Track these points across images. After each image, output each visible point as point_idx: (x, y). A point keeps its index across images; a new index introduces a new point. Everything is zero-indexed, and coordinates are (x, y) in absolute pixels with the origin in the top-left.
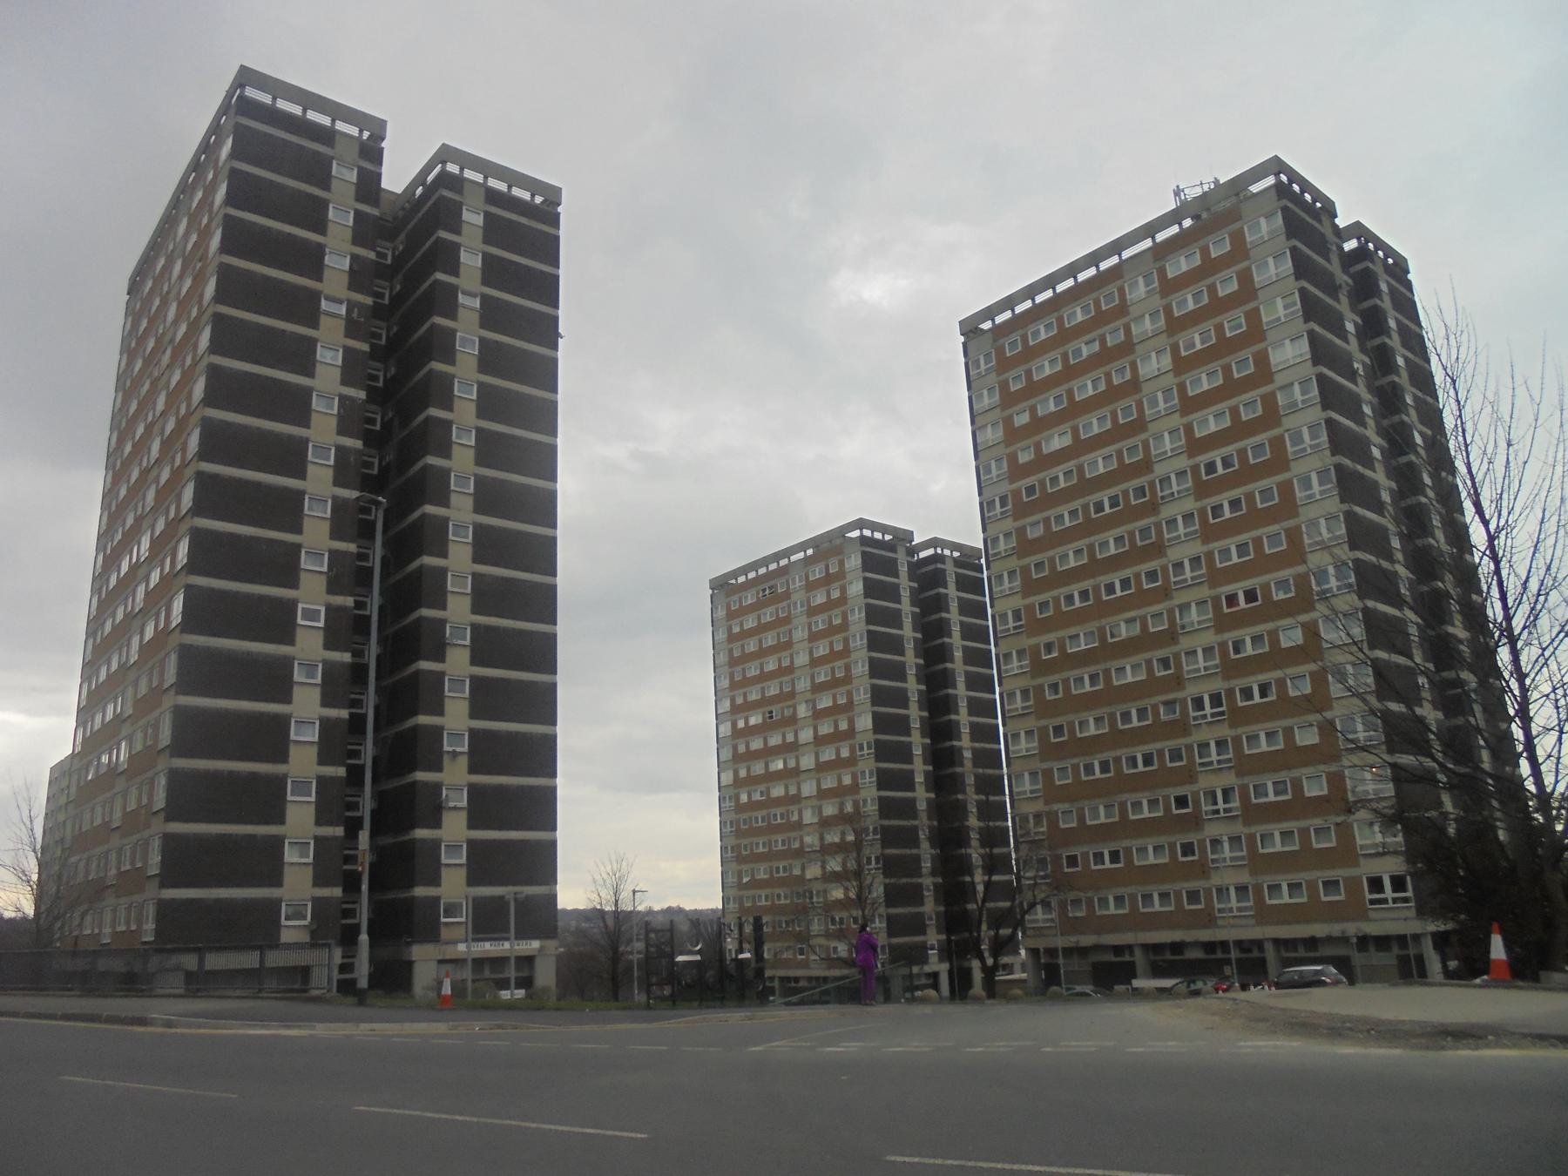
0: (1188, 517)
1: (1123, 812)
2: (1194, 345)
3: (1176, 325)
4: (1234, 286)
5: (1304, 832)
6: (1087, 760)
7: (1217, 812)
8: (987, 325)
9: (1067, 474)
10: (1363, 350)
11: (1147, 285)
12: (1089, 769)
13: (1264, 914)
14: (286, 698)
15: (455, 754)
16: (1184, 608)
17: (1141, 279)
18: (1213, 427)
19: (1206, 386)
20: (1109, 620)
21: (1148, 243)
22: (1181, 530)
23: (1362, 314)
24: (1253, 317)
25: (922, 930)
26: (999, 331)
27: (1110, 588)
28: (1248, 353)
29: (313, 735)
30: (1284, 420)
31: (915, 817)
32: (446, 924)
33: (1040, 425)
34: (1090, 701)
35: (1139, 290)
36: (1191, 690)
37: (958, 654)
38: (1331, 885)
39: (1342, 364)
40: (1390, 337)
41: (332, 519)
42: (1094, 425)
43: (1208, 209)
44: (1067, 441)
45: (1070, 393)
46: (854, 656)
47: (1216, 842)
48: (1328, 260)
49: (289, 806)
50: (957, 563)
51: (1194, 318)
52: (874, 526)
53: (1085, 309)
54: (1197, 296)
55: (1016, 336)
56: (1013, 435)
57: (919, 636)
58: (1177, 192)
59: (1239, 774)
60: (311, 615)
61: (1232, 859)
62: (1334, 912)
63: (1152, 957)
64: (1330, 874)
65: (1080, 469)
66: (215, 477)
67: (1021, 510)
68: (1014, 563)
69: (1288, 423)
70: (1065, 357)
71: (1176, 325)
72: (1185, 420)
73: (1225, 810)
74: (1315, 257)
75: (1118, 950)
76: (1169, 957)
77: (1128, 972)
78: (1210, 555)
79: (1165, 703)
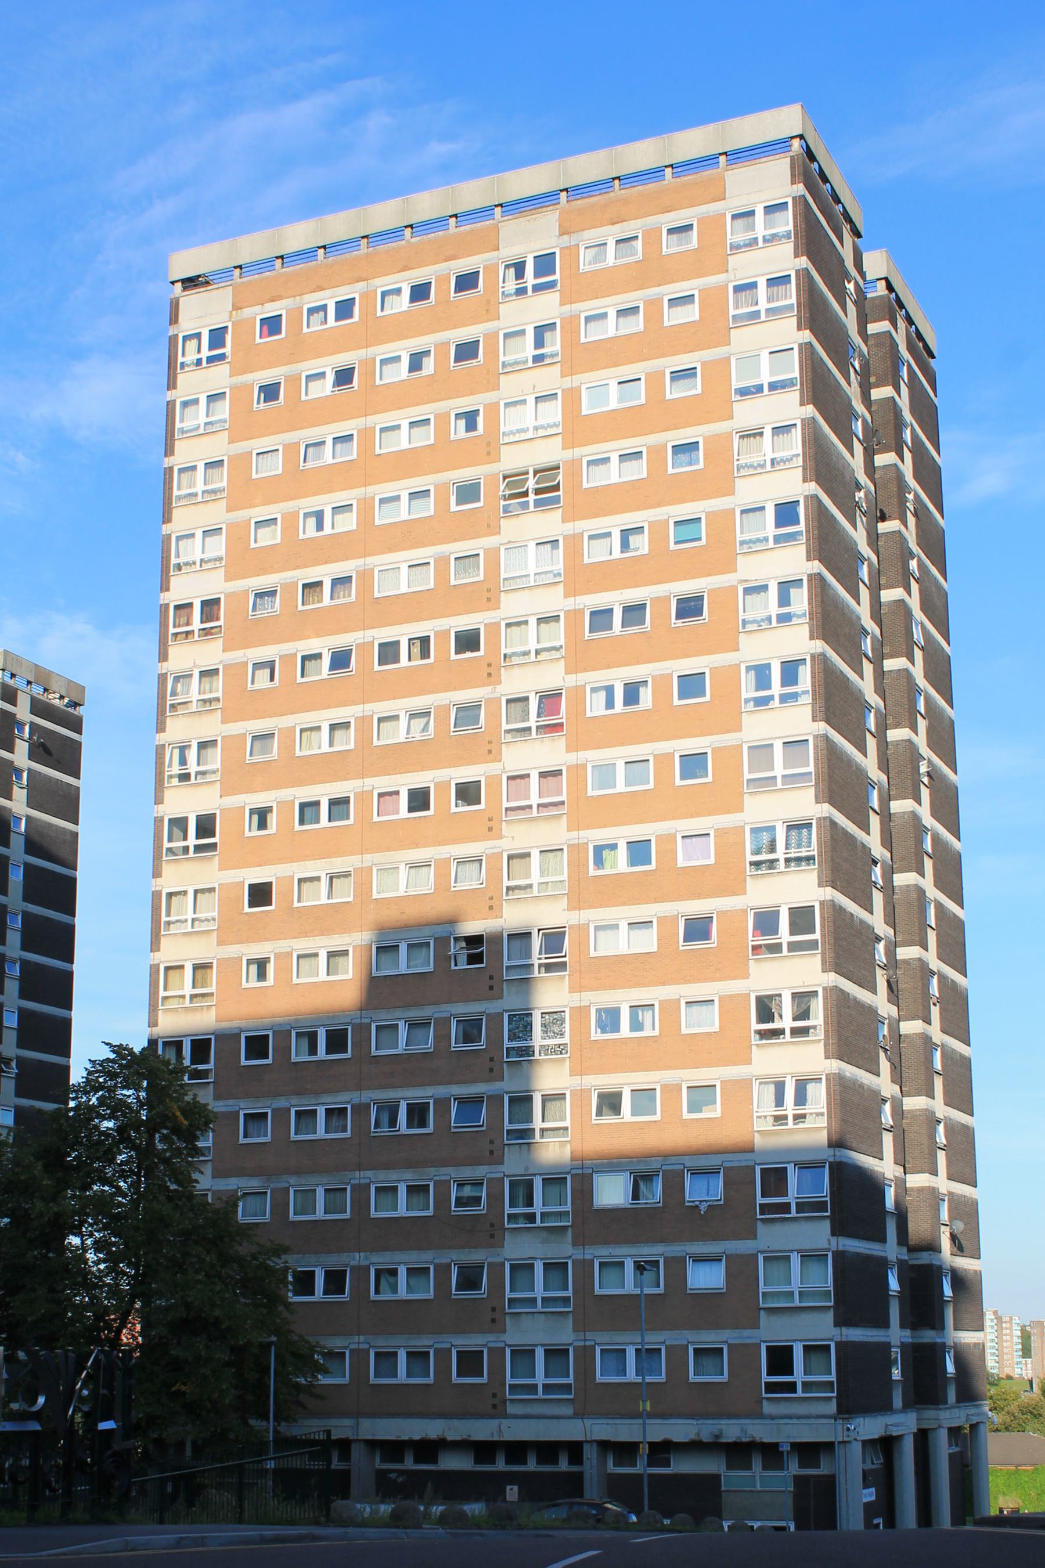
7: (531, 1218)
13: (591, 1400)
32: (512, 1401)
38: (707, 1354)
62: (709, 1402)
63: (379, 1465)
64: (709, 1338)
76: (409, 1463)
77: (340, 1485)
79: (462, 1101)
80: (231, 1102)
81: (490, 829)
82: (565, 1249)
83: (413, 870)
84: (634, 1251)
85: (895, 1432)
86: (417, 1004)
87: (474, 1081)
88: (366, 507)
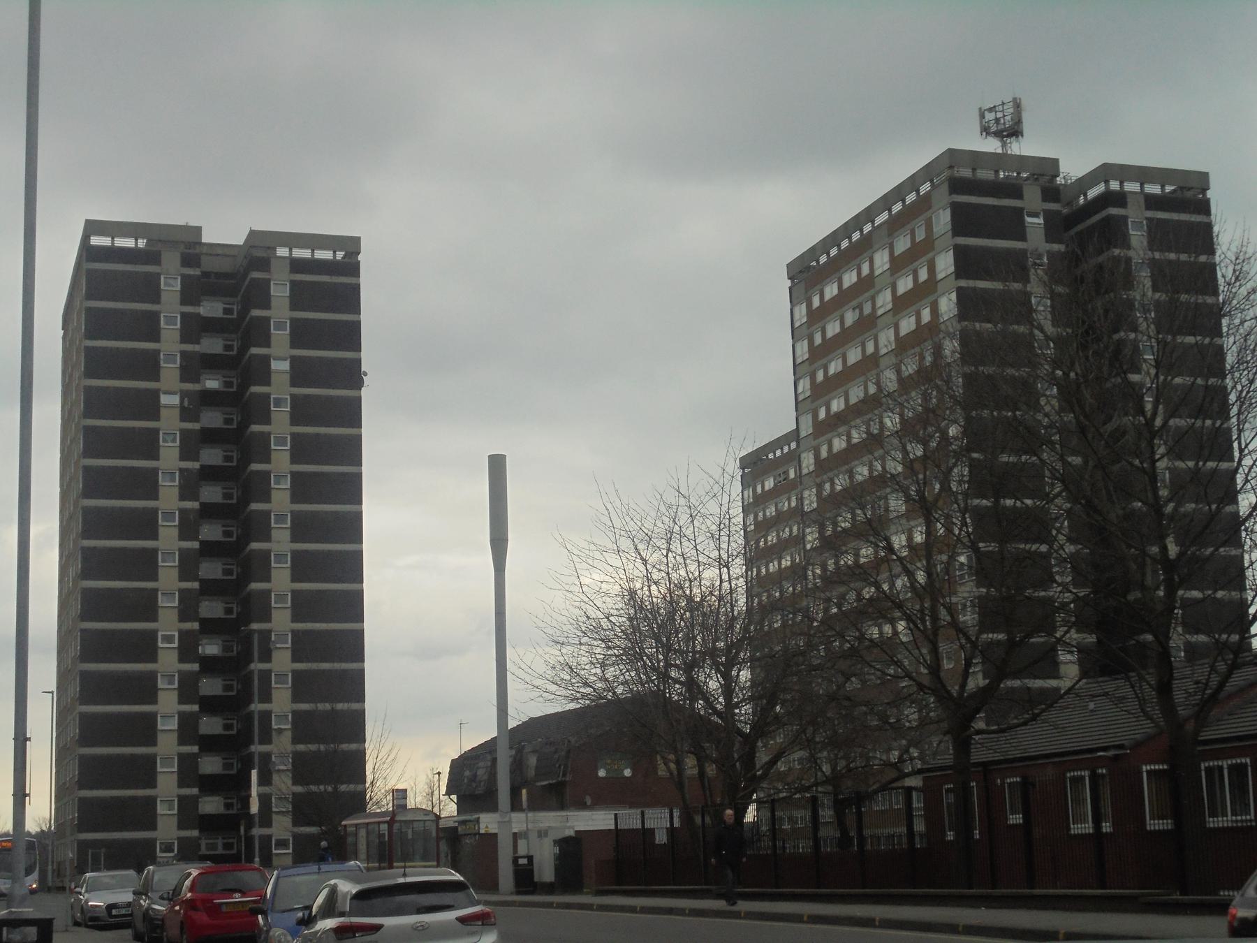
14: (154, 701)
15: (280, 731)
29: (173, 725)
32: (277, 855)
41: (180, 566)
49: (160, 652)
60: (169, 639)
66: (94, 428)
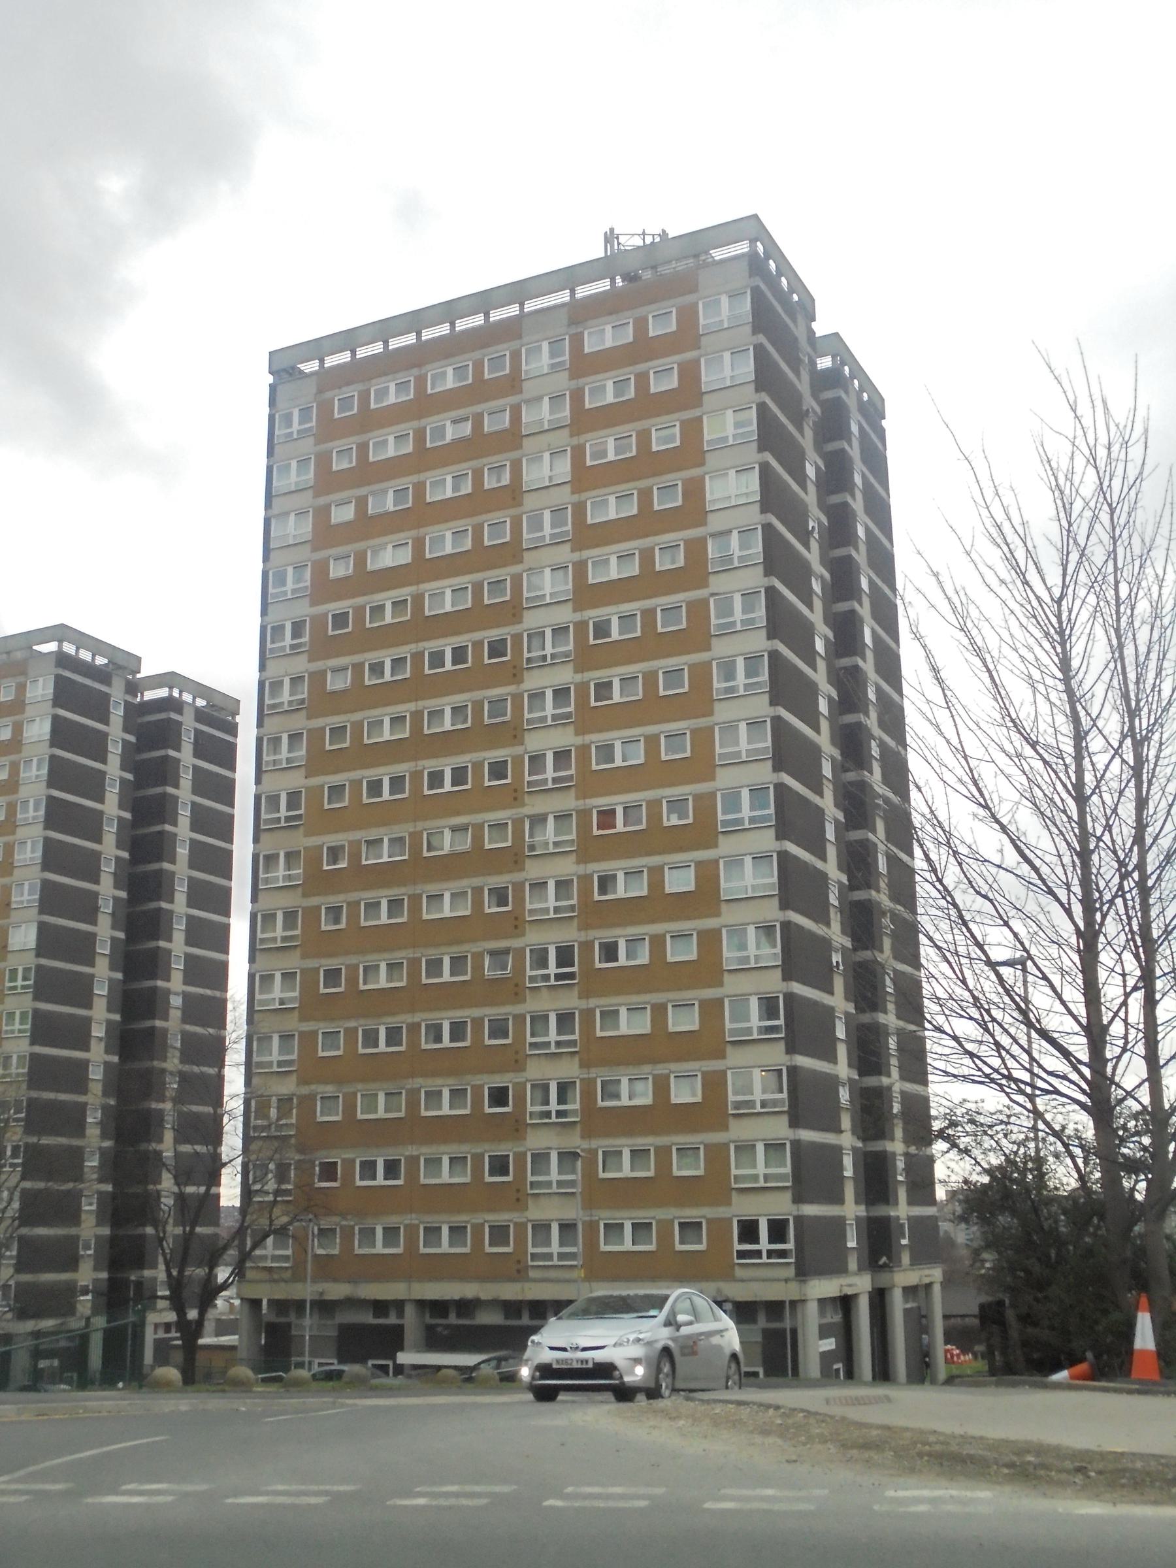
0: (561, 694)
1: (413, 1104)
2: (604, 453)
3: (585, 420)
4: (672, 382)
5: (663, 1153)
6: (370, 1024)
7: (548, 1114)
8: (311, 367)
9: (398, 605)
10: (821, 505)
11: (553, 355)
12: (371, 1038)
16: (539, 820)
17: (545, 346)
18: (614, 572)
19: (612, 515)
20: (429, 824)
21: (563, 297)
22: (550, 709)
23: (825, 456)
24: (692, 430)
25: (72, 1263)
26: (330, 379)
27: (436, 779)
28: (677, 479)
30: (712, 579)
31: (85, 1091)
32: (533, 1266)
33: (369, 526)
34: (384, 938)
35: (540, 361)
36: (533, 938)
37: (183, 852)
38: (690, 1228)
39: (795, 517)
40: (853, 496)
42: (447, 541)
43: (654, 267)
44: (405, 557)
45: (420, 488)
46: (21, 833)
47: (540, 1159)
48: (798, 374)
50: (201, 716)
51: (609, 417)
52: (82, 640)
53: (460, 371)
54: (619, 385)
55: (353, 391)
56: (326, 534)
57: (127, 815)
58: (610, 237)
59: (585, 1065)
61: (560, 1184)
63: (429, 1320)
64: (691, 1214)
65: (418, 599)
67: (324, 646)
68: (300, 722)
69: (718, 584)
70: (420, 436)
71: (585, 420)
72: (576, 556)
73: (560, 1114)
74: (783, 365)
75: (380, 1307)
77: (393, 1340)
78: (584, 750)
79: (493, 953)
80: (311, 1023)
81: (515, 799)
82: (575, 1141)
83: (457, 833)
84: (630, 1141)
85: (849, 1291)
86: (459, 942)
87: (503, 1004)
88: (417, 716)
